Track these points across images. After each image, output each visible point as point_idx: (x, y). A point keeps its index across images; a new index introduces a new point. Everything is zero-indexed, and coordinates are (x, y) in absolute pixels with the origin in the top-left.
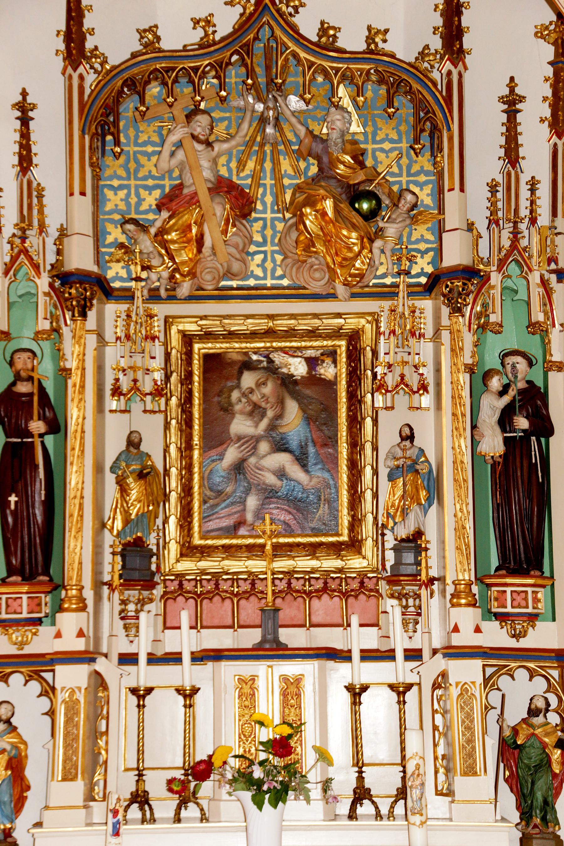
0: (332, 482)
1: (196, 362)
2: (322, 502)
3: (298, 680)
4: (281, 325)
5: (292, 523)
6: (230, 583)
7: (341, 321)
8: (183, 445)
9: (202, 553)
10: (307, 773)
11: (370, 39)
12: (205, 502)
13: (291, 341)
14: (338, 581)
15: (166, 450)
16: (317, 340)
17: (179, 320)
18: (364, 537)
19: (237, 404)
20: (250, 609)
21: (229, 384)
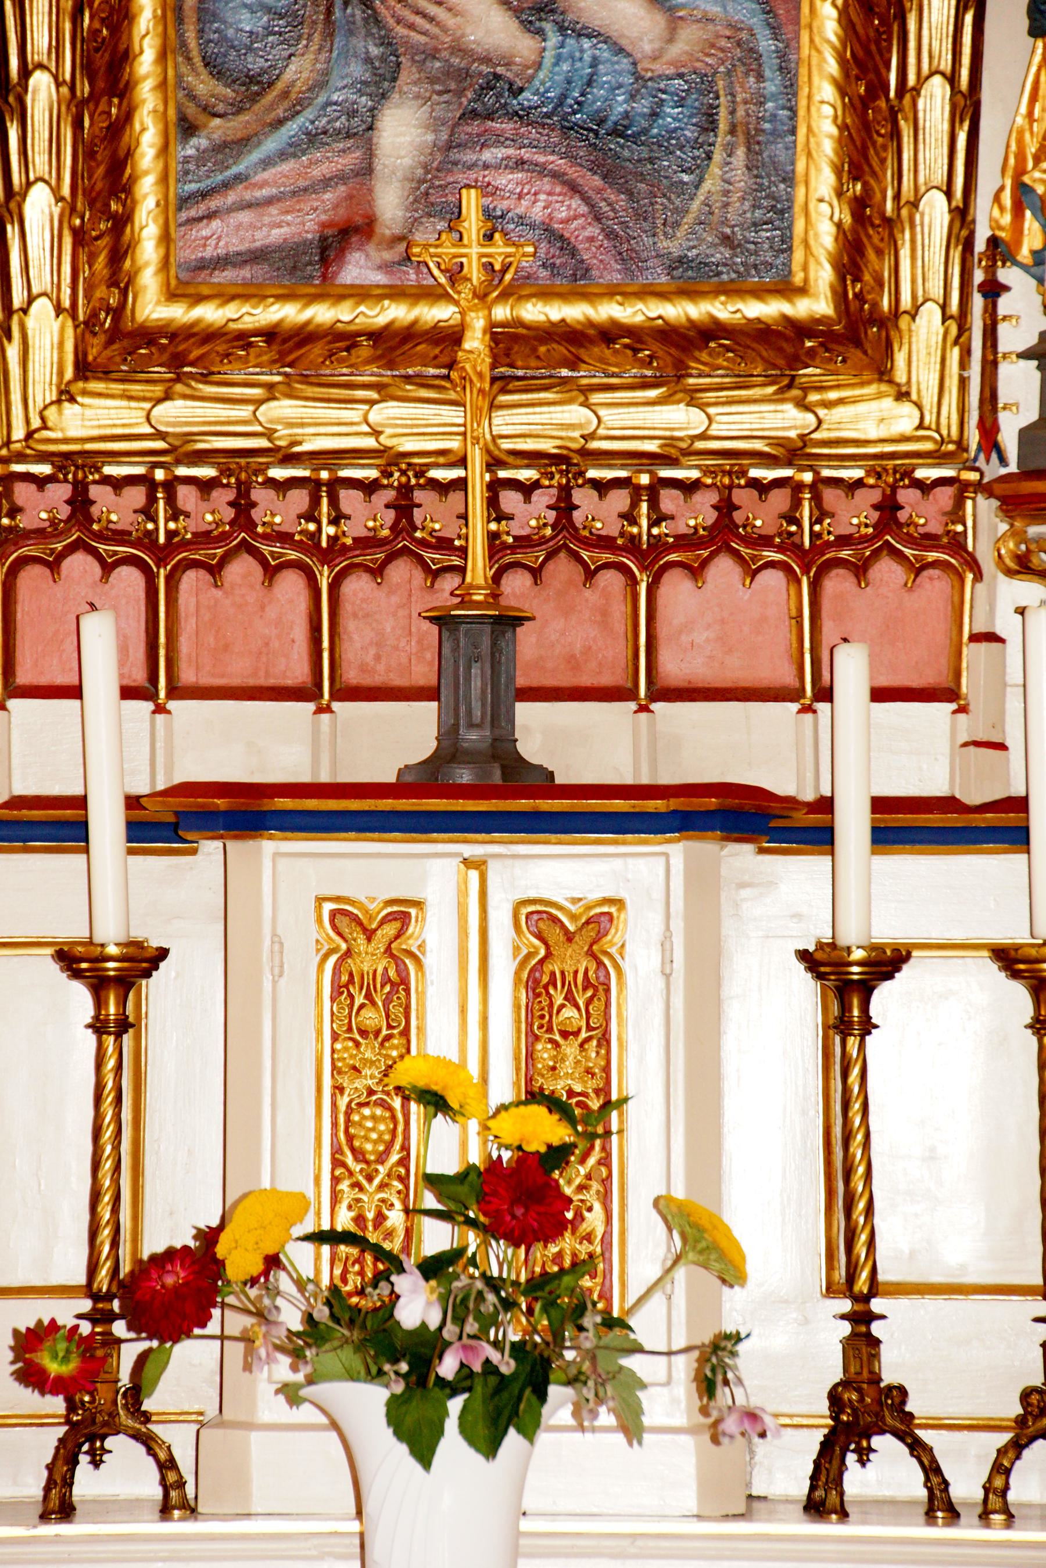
0: (766, 44)
2: (722, 138)
3: (598, 923)
5: (584, 232)
6: (299, 499)
9: (176, 362)
10: (630, 1311)
12: (188, 128)
14: (780, 500)
18: (906, 302)
20: (388, 619)
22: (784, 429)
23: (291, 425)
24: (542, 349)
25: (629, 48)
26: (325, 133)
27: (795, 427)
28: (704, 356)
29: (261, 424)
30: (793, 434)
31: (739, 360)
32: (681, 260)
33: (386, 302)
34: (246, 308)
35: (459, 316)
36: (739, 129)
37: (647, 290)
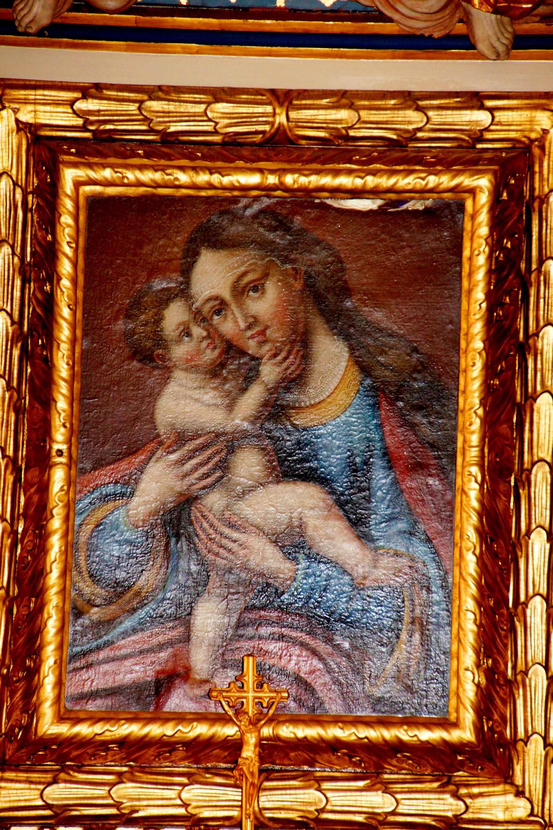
1: (66, 219)
2: (405, 627)
4: (310, 124)
7: (482, 117)
8: (23, 452)
9: (61, 759)
13: (336, 173)
16: (410, 172)
17: (21, 94)
19: (179, 341)
21: (159, 284)
22: (444, 811)
23: (132, 800)
24: (292, 754)
25: (349, 571)
26: (161, 616)
27: (451, 810)
28: (394, 762)
29: (113, 799)
30: (450, 814)
31: (416, 765)
32: (379, 700)
33: (195, 724)
34: (107, 727)
35: (239, 733)
36: (416, 621)
37: (358, 720)
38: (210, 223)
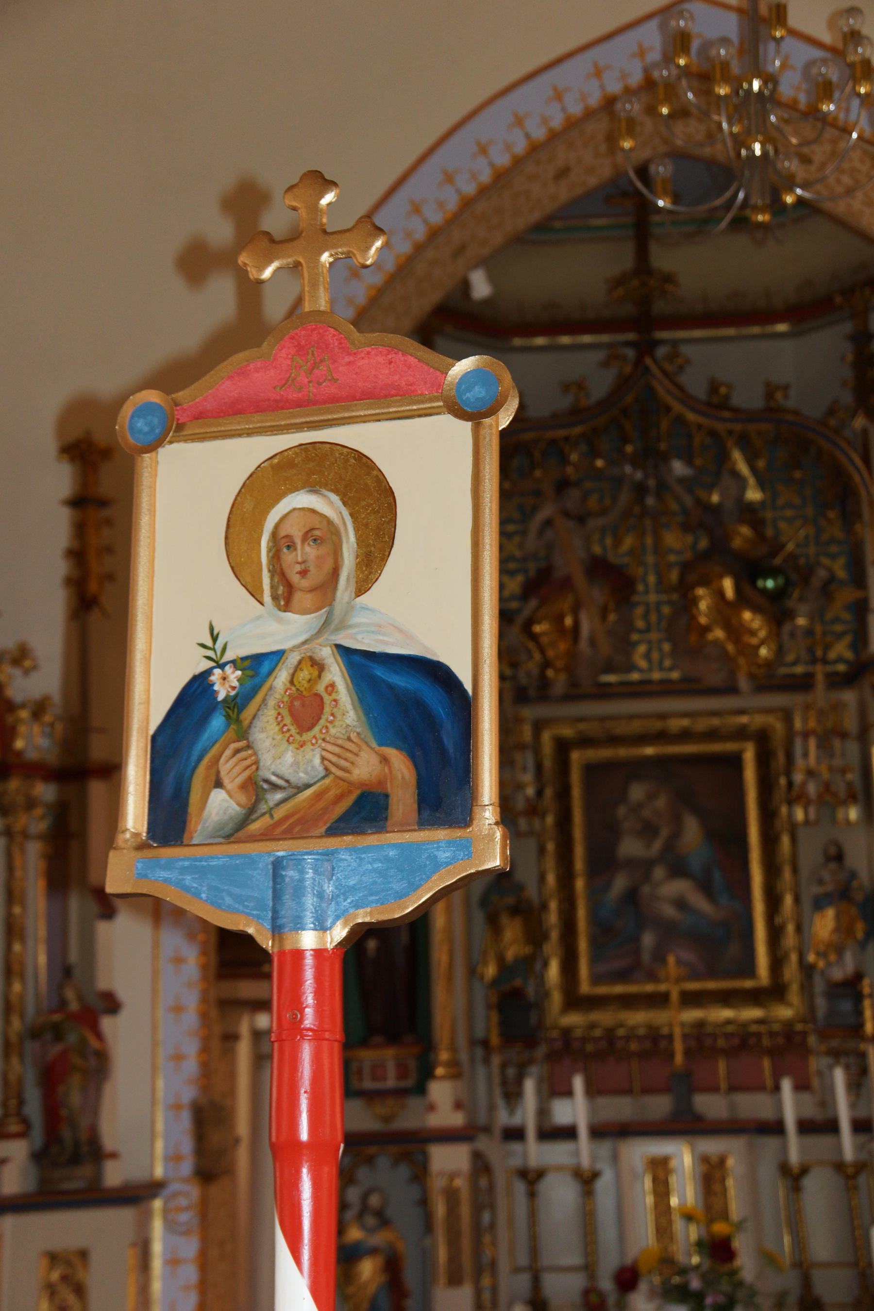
11: (769, 394)
15: (542, 878)
38: (637, 769)
